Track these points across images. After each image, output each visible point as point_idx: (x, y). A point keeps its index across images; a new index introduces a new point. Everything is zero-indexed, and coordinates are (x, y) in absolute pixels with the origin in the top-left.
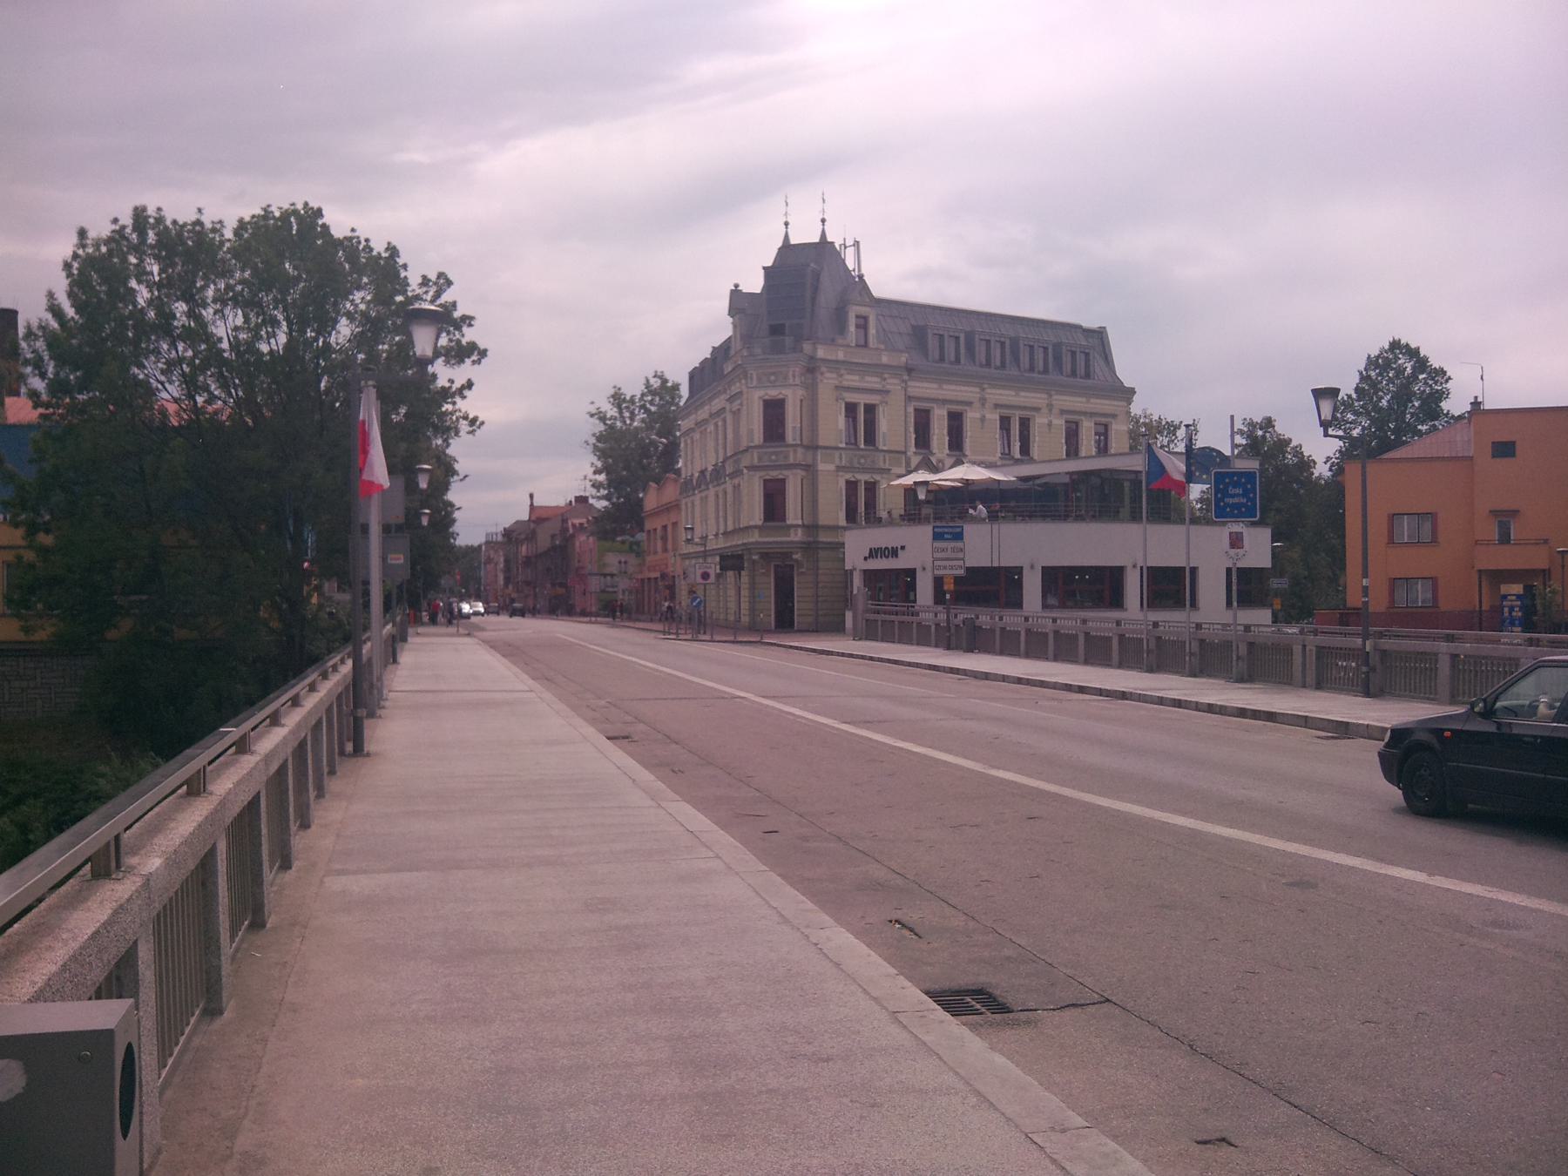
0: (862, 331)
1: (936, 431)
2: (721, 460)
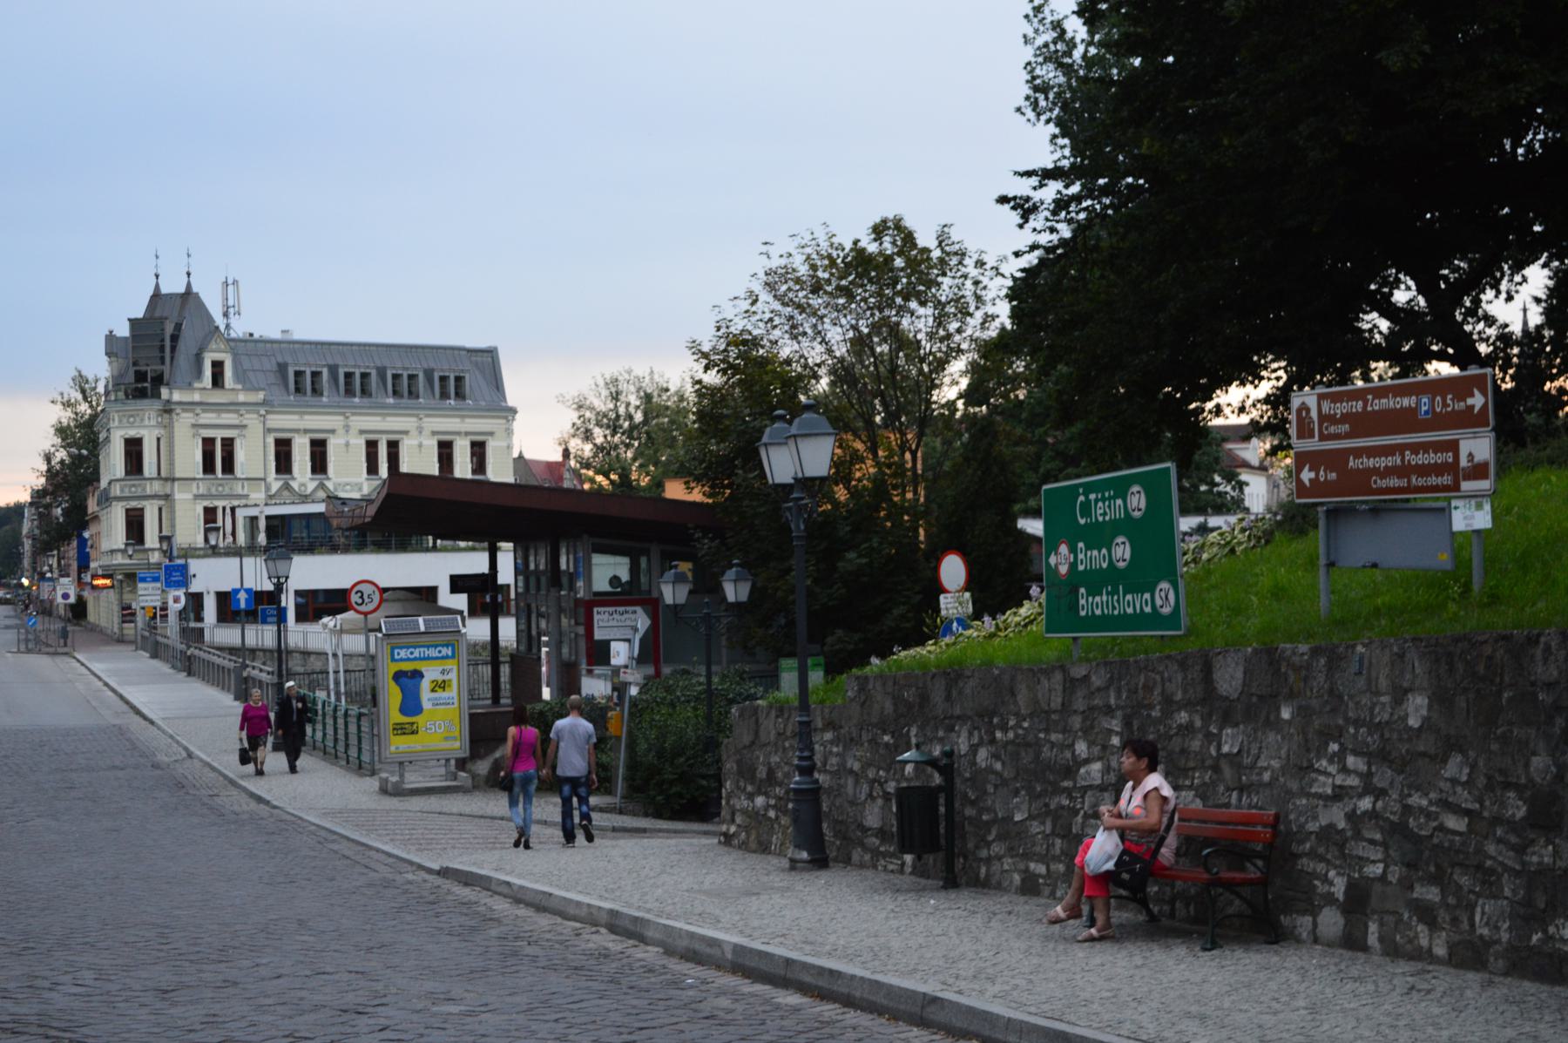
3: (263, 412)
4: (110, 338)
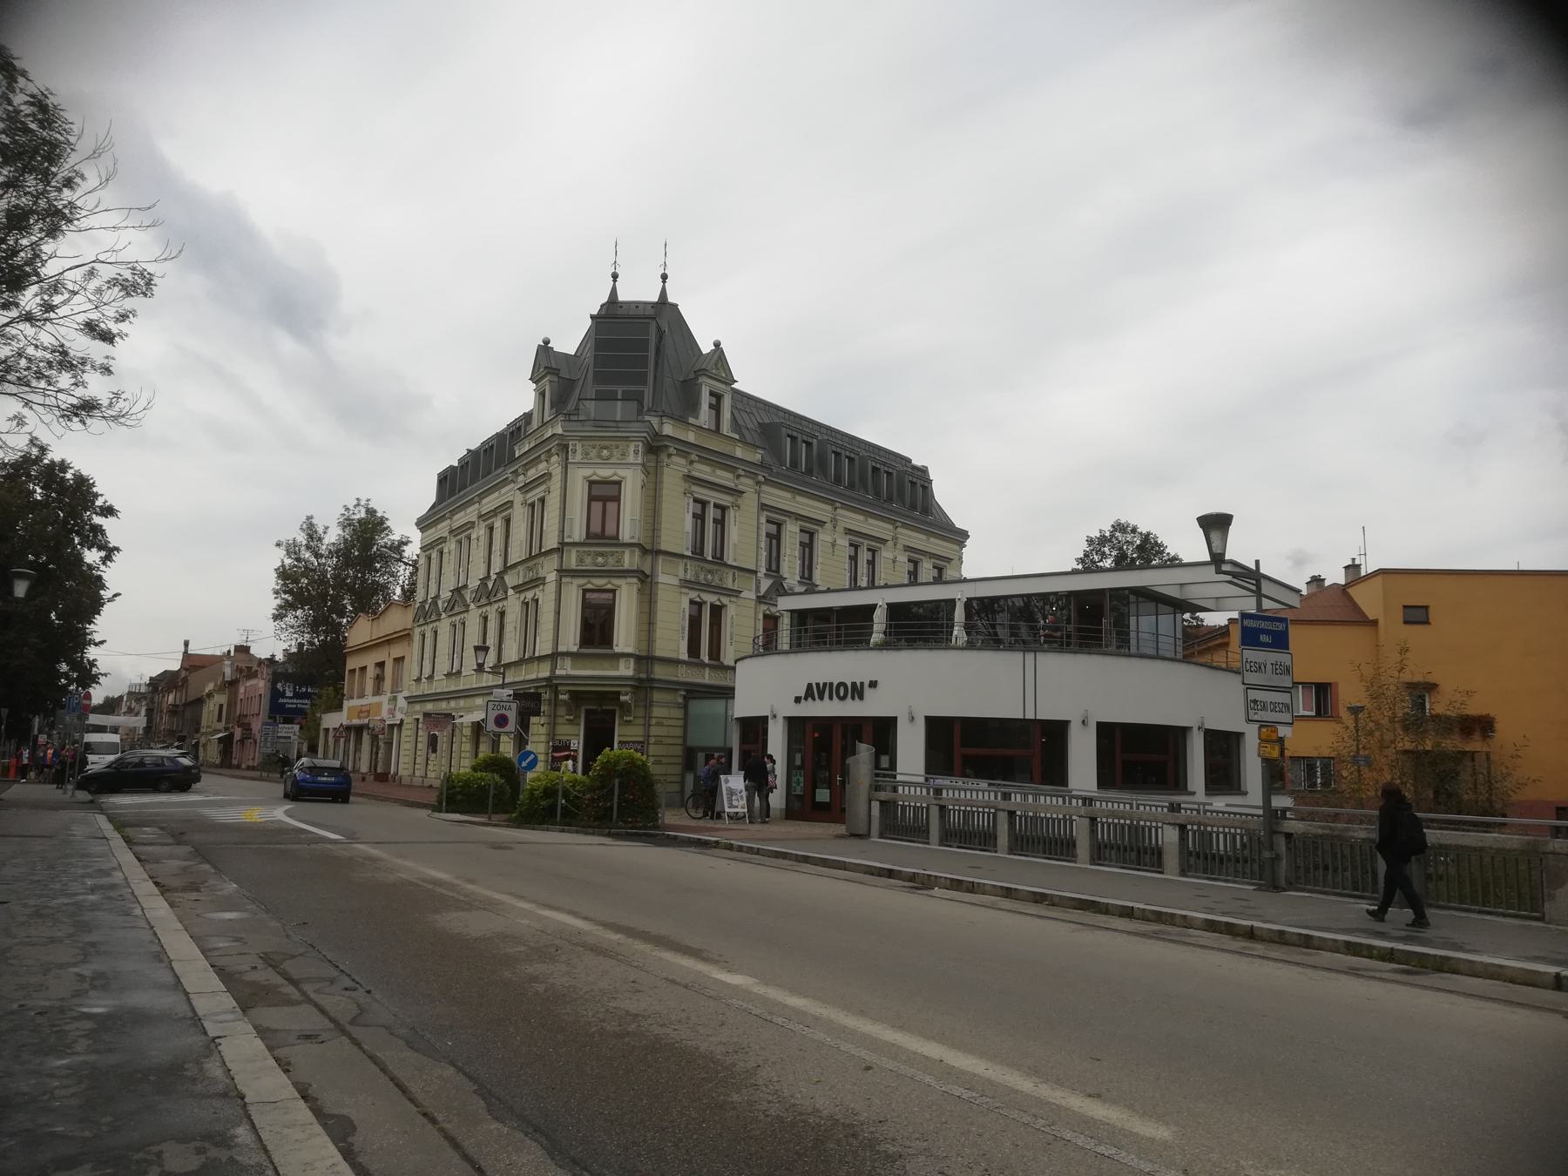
0: (714, 412)
3: (761, 478)
4: (545, 350)
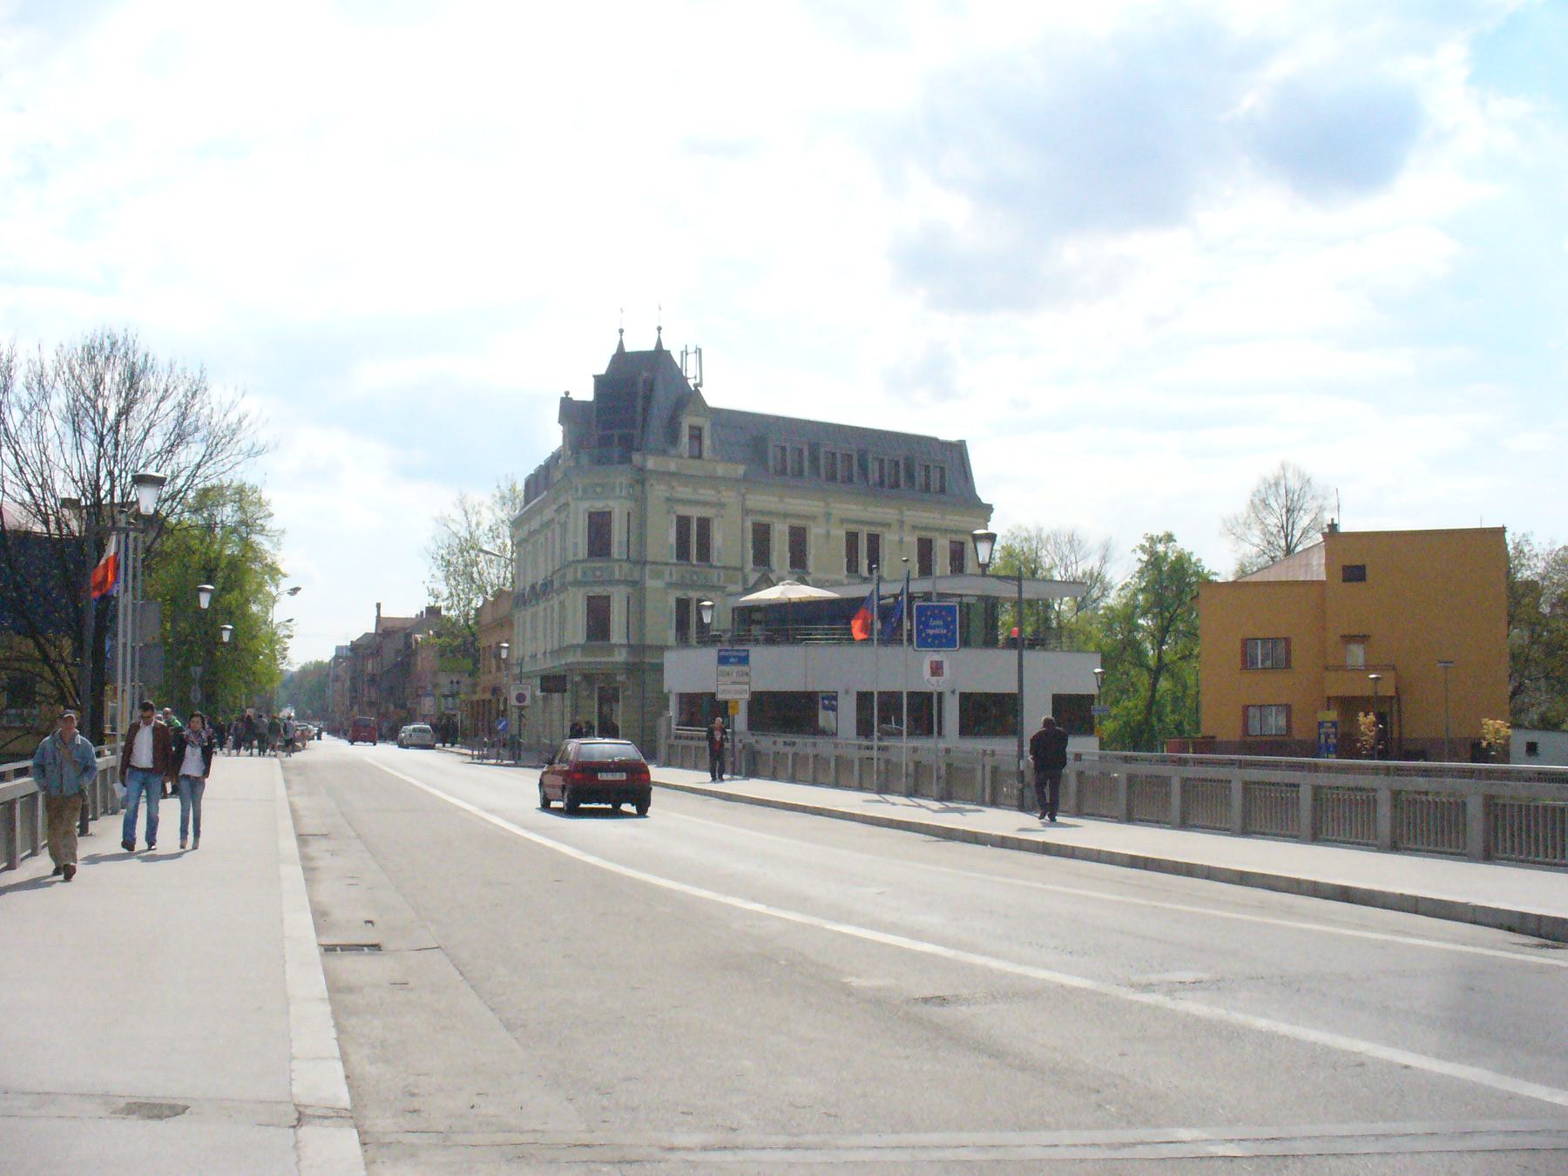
0: (696, 443)
1: (777, 547)
2: (549, 574)
